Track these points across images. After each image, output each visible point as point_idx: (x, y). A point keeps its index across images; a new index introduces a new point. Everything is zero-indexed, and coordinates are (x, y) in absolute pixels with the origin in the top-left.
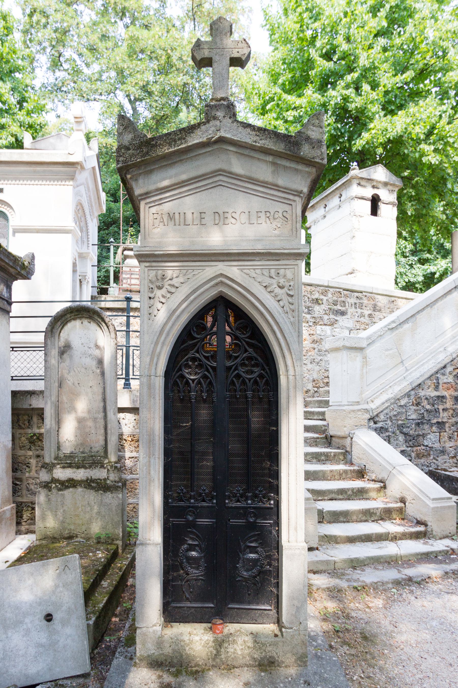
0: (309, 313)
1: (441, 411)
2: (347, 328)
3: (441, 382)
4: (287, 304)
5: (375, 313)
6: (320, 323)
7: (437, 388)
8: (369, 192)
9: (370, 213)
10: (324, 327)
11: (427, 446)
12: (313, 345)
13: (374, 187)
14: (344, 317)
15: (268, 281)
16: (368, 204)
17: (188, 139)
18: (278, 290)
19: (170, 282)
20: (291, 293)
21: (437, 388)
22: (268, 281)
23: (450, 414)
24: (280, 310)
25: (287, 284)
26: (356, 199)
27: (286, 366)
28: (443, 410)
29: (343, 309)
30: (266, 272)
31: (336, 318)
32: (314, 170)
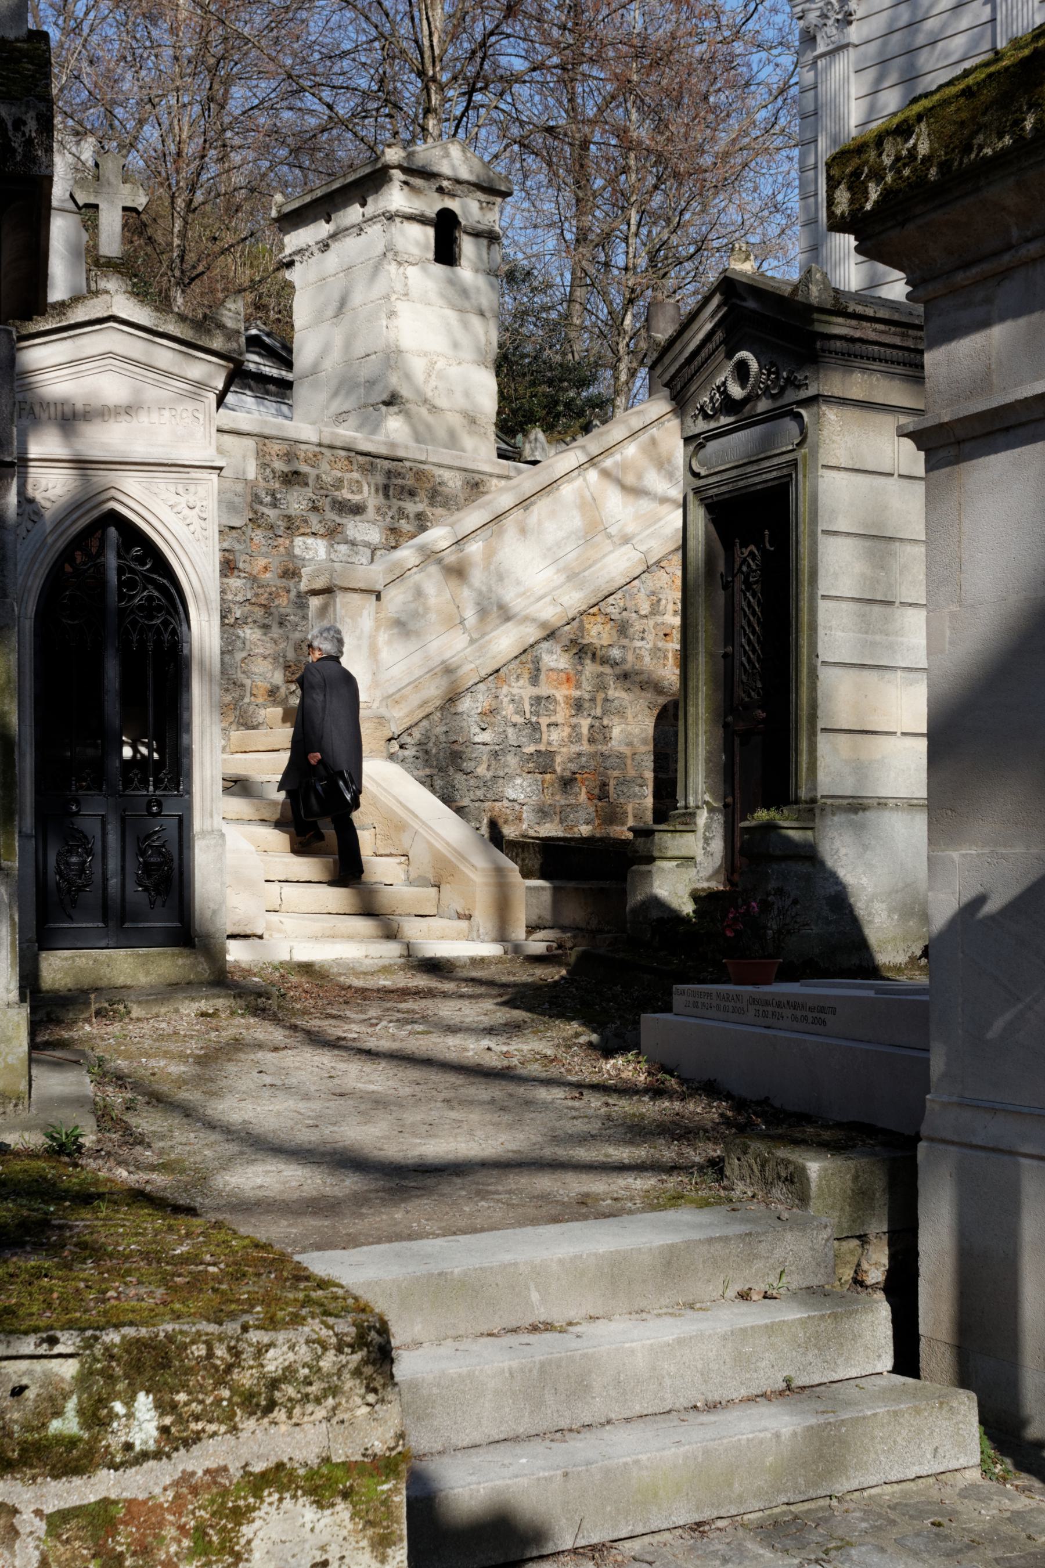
0: (275, 506)
1: (544, 728)
2: (367, 545)
3: (543, 666)
4: (199, 530)
5: (434, 510)
6: (302, 530)
7: (535, 680)
8: (432, 205)
9: (431, 255)
10: (310, 541)
11: (514, 801)
12: (283, 582)
13: (440, 190)
14: (358, 518)
15: (174, 499)
16: (427, 235)
17: (69, 314)
18: (186, 511)
19: (45, 494)
20: (204, 515)
21: (535, 680)
22: (174, 499)
23: (565, 734)
24: (191, 537)
25: (199, 504)
26: (398, 220)
27: (622, 1168)
28: (549, 725)
29: (356, 498)
30: (172, 488)
31: (338, 520)
32: (231, 365)
